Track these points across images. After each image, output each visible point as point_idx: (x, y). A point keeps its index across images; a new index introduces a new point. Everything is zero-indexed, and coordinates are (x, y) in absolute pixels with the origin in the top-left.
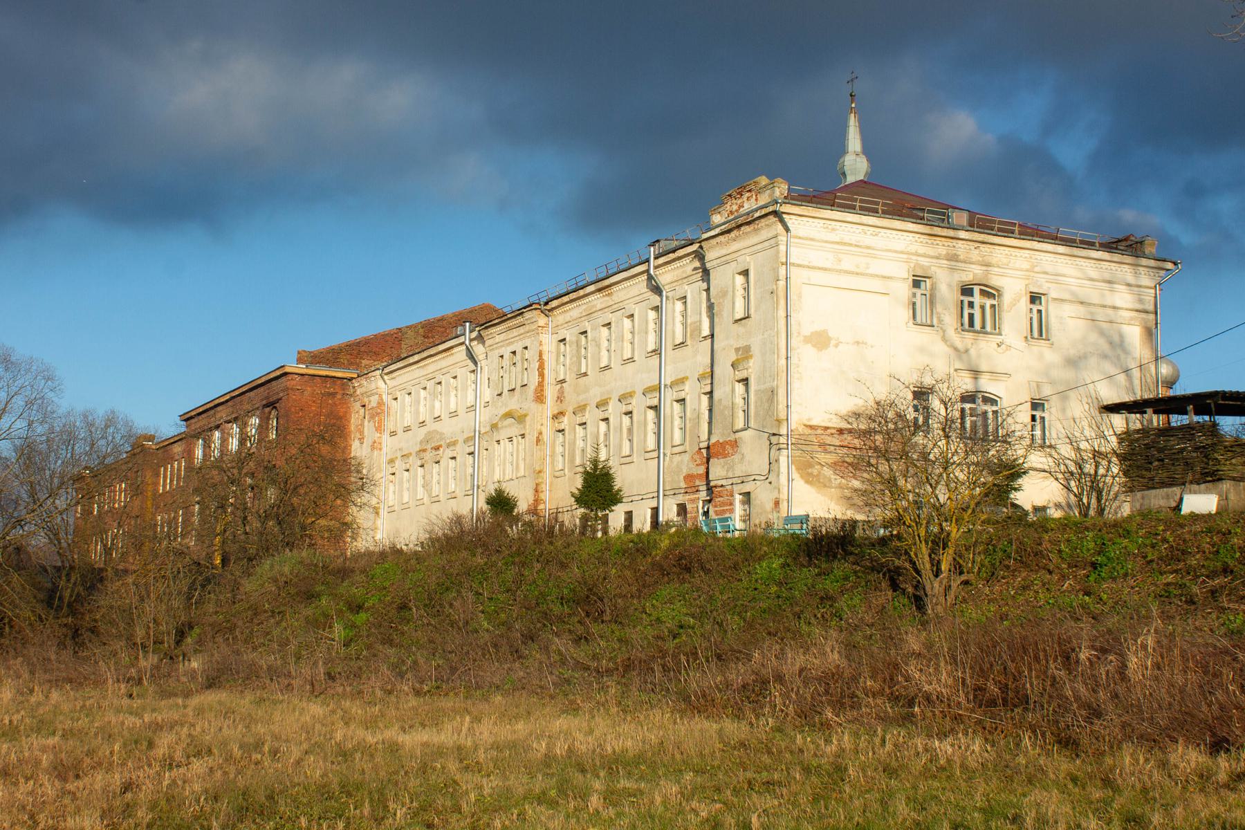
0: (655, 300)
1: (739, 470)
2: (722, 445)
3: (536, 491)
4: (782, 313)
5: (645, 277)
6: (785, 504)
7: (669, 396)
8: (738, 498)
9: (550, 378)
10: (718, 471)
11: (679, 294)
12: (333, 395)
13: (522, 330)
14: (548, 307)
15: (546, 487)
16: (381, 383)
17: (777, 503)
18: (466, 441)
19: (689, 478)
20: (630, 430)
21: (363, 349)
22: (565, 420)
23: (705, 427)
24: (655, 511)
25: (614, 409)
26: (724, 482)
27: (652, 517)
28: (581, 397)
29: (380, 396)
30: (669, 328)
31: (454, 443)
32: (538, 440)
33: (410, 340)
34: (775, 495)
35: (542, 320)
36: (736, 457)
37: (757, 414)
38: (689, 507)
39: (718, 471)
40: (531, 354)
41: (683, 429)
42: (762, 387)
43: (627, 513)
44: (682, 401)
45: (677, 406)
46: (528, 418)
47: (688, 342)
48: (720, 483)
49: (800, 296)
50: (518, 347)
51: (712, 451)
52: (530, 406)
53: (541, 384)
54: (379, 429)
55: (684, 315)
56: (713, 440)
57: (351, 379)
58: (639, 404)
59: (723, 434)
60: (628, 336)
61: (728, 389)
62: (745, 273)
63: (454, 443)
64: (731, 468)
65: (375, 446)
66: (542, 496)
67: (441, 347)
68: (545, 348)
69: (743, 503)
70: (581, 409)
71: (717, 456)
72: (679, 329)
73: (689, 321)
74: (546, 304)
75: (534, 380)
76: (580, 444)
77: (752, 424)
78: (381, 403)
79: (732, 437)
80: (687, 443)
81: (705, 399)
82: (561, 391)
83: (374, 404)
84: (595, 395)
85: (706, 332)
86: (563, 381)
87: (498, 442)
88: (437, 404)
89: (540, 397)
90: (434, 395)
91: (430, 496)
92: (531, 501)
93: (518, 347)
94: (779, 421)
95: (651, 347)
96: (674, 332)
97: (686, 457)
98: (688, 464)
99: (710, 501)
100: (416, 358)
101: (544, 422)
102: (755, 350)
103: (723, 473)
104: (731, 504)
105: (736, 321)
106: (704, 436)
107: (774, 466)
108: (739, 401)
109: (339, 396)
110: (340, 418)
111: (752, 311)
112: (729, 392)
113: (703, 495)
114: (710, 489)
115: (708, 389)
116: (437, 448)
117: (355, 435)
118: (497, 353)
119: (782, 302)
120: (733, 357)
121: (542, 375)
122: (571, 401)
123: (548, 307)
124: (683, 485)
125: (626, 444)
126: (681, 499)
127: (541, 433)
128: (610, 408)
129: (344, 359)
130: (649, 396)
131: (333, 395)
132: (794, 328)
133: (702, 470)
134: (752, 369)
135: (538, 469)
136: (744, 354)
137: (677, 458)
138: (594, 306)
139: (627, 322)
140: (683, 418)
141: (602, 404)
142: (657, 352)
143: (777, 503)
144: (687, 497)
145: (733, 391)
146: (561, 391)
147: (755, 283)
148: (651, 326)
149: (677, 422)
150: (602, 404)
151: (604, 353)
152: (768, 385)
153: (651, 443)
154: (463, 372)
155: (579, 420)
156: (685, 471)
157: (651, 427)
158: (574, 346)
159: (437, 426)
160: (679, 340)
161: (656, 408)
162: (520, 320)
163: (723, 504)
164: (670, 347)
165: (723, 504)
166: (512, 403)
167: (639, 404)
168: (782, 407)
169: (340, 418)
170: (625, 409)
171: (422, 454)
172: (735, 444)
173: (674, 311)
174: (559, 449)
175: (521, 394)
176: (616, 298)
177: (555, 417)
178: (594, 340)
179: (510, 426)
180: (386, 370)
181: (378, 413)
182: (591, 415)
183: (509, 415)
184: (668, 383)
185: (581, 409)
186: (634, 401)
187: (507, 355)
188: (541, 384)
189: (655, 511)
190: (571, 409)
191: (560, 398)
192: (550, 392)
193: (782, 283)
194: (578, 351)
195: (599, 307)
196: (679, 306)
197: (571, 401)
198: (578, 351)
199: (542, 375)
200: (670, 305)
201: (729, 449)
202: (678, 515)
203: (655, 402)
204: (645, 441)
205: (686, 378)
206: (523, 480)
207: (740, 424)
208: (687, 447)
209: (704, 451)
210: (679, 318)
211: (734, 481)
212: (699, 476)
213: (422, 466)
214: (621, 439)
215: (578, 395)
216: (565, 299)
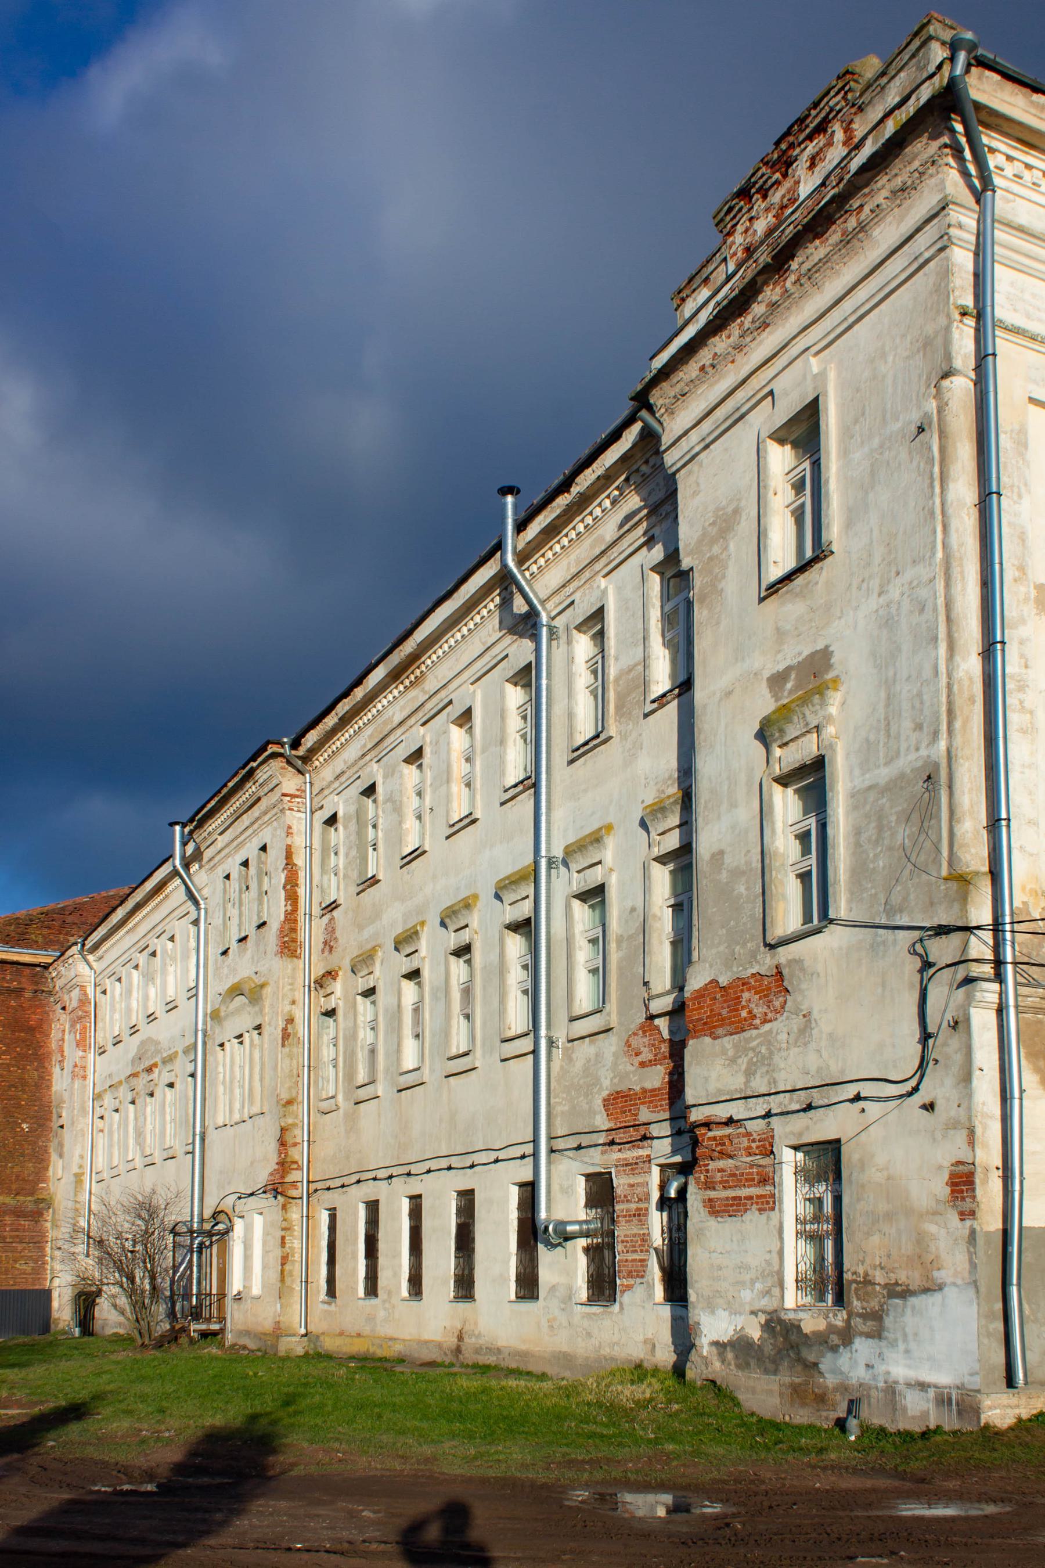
0: (521, 650)
1: (794, 1068)
2: (728, 995)
3: (282, 1143)
4: (963, 490)
5: (494, 601)
6: (996, 1185)
7: (562, 885)
8: (789, 1159)
9: (308, 901)
10: (714, 1074)
11: (583, 609)
12: (18, 992)
13: (256, 812)
14: (301, 751)
15: (300, 1134)
16: (82, 968)
17: (962, 1182)
18: (186, 1052)
19: (619, 1101)
20: (467, 992)
21: (69, 919)
22: (338, 987)
23: (662, 956)
24: (529, 1191)
25: (433, 945)
26: (736, 1110)
27: (521, 1207)
28: (368, 932)
29: (83, 988)
30: (559, 710)
31: (169, 1060)
32: (286, 1036)
33: (680, 1311)
34: (954, 1149)
35: (290, 782)
36: (781, 1028)
37: (860, 871)
38: (620, 1183)
39: (714, 1074)
40: (275, 858)
41: (600, 972)
42: (884, 774)
43: (411, 1198)
44: (594, 895)
45: (581, 912)
46: (268, 991)
47: (612, 730)
48: (722, 1112)
49: (1022, 444)
50: (250, 850)
51: (692, 1014)
52: (277, 968)
53: (291, 918)
54: (81, 1044)
55: (598, 669)
56: (696, 982)
57: (46, 967)
58: (485, 923)
59: (730, 960)
60: (459, 768)
61: (746, 813)
62: (804, 430)
63: (169, 1060)
64: (764, 1062)
65: (79, 1072)
66: (294, 1154)
67: (149, 885)
68: (299, 841)
69: (805, 1175)
70: (364, 960)
71: (710, 1028)
72: (584, 708)
73: (612, 672)
74: (295, 744)
75: (276, 910)
76: (365, 1036)
77: (841, 906)
78: (84, 1001)
79: (765, 963)
80: (612, 1006)
81: (662, 877)
82: (331, 930)
83: (75, 1004)
84: (394, 920)
85: (661, 680)
86: (333, 906)
87: (222, 1045)
88: (152, 992)
89: (289, 947)
90: (149, 978)
91: (142, 1150)
92: (272, 1165)
93: (250, 850)
94: (962, 881)
95: (514, 773)
96: (570, 716)
97: (610, 1045)
98: (620, 1065)
99: (685, 1169)
100: (120, 913)
101: (298, 995)
102: (852, 660)
103: (736, 1082)
104: (765, 1180)
105: (774, 588)
106: (662, 979)
107: (946, 1046)
108: (785, 846)
109: (28, 995)
110: (32, 1030)
111: (834, 531)
112: (750, 820)
113: (662, 1149)
114: (687, 1134)
115: (673, 841)
116: (149, 1070)
117: (56, 1057)
118: (220, 872)
119: (965, 452)
120: (764, 704)
121: (292, 898)
122: (349, 944)
123: (301, 751)
124: (602, 1121)
125: (459, 1026)
126: (597, 1160)
127: (290, 1021)
128: (424, 945)
129: (35, 934)
130: (509, 897)
131: (18, 992)
132: (1008, 550)
133: (657, 1077)
134: (841, 727)
135: (285, 1096)
136: (812, 678)
137: (586, 1049)
138: (390, 719)
139: (457, 736)
140: (599, 942)
141: (406, 940)
142: (531, 783)
143: (962, 1182)
144: (615, 1155)
145: (764, 813)
146: (331, 930)
147: (847, 433)
148: (514, 723)
149: (584, 955)
150: (406, 940)
151: (410, 823)
152: (908, 761)
153: (517, 1019)
154: (182, 928)
155: (362, 984)
156: (607, 1084)
157: (516, 976)
158: (353, 826)
159: (147, 1031)
160: (585, 730)
161: (525, 927)
162: (251, 788)
163: (736, 1179)
164: (561, 756)
165: (736, 1179)
166: (243, 966)
167: (485, 923)
168: (972, 826)
169: (32, 1030)
170: (454, 940)
171: (134, 1081)
172: (776, 985)
173: (570, 660)
174: (327, 1053)
175: (257, 944)
176: (431, 684)
177: (320, 983)
178: (390, 799)
179: (238, 1011)
180: (89, 944)
181: (84, 1014)
182: (387, 969)
183: (236, 991)
184: (558, 852)
185: (364, 960)
186: (474, 920)
187: (236, 871)
188: (291, 918)
189: (529, 1191)
190: (346, 964)
191: (328, 946)
192: (311, 932)
193: (961, 387)
194: (361, 833)
195: (397, 719)
196: (583, 646)
197: (349, 944)
198: (361, 833)
199: (292, 898)
200: (559, 652)
201: (753, 1002)
202: (590, 1204)
203: (525, 910)
204: (502, 1011)
205: (609, 828)
206: (260, 1121)
207: (788, 915)
208: (612, 1015)
209: (663, 1024)
210: (583, 679)
211: (775, 1104)
212: (648, 1096)
213: (133, 1102)
214: (448, 1017)
215: (361, 928)
216: (331, 721)
